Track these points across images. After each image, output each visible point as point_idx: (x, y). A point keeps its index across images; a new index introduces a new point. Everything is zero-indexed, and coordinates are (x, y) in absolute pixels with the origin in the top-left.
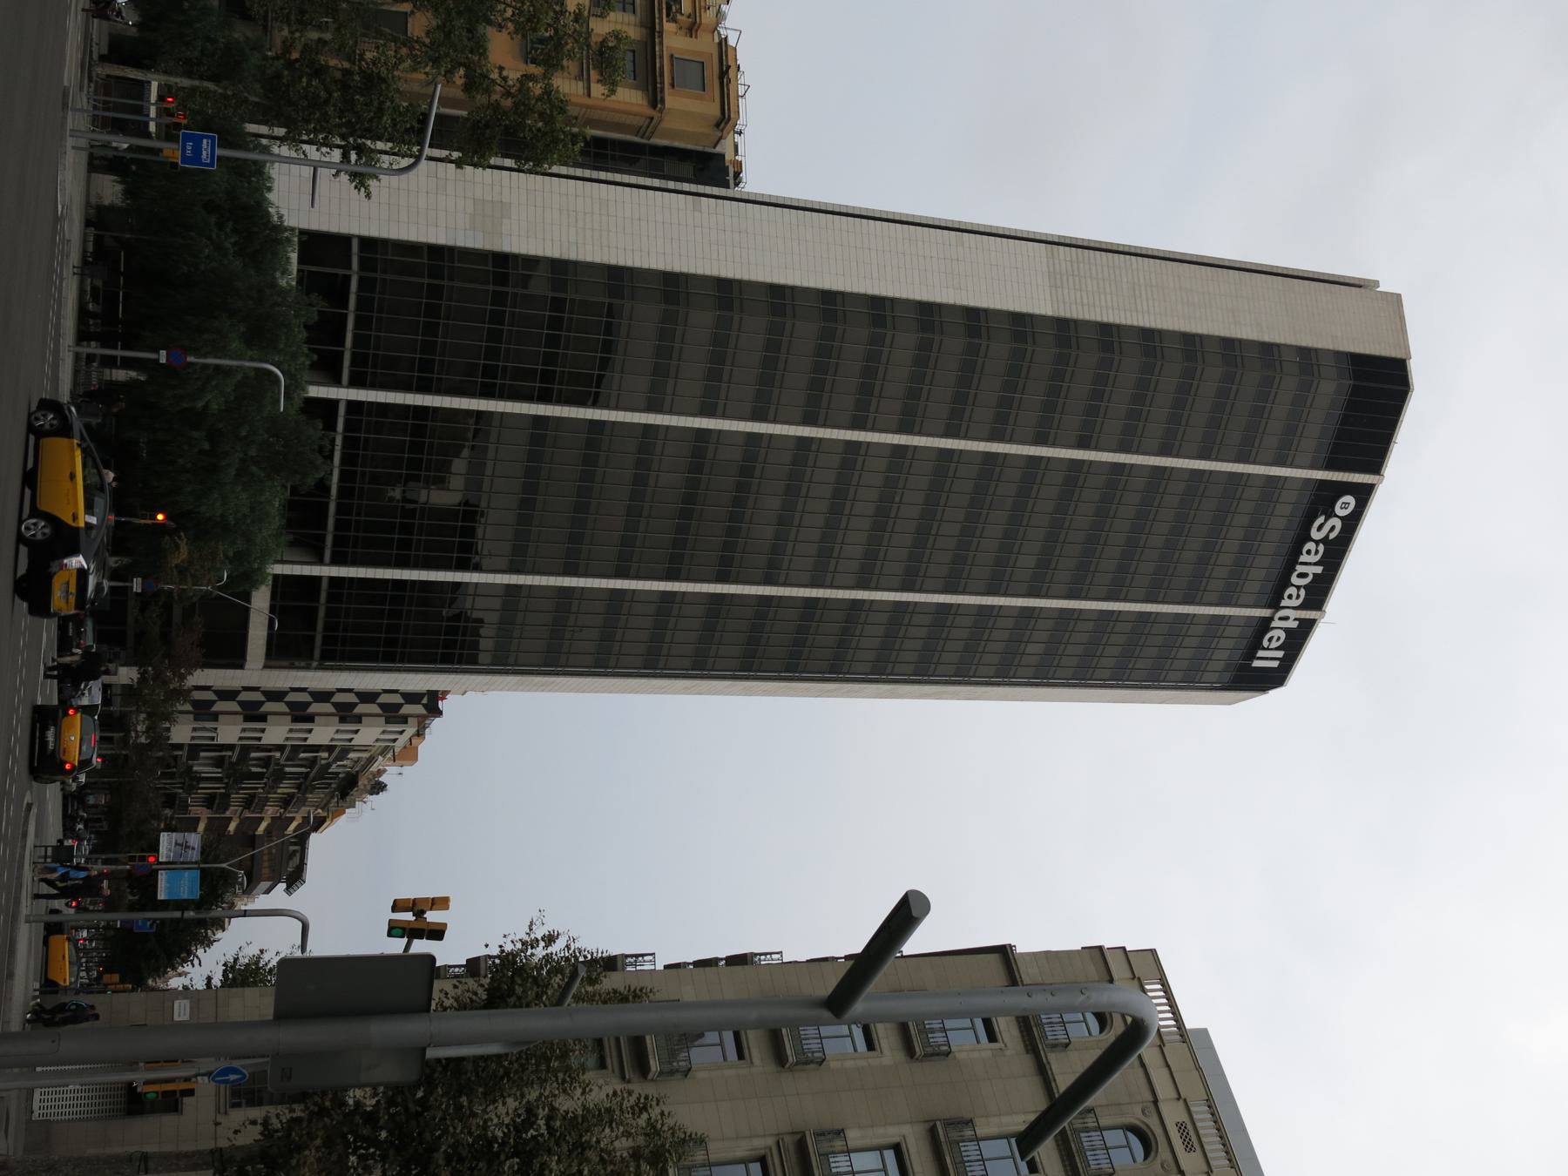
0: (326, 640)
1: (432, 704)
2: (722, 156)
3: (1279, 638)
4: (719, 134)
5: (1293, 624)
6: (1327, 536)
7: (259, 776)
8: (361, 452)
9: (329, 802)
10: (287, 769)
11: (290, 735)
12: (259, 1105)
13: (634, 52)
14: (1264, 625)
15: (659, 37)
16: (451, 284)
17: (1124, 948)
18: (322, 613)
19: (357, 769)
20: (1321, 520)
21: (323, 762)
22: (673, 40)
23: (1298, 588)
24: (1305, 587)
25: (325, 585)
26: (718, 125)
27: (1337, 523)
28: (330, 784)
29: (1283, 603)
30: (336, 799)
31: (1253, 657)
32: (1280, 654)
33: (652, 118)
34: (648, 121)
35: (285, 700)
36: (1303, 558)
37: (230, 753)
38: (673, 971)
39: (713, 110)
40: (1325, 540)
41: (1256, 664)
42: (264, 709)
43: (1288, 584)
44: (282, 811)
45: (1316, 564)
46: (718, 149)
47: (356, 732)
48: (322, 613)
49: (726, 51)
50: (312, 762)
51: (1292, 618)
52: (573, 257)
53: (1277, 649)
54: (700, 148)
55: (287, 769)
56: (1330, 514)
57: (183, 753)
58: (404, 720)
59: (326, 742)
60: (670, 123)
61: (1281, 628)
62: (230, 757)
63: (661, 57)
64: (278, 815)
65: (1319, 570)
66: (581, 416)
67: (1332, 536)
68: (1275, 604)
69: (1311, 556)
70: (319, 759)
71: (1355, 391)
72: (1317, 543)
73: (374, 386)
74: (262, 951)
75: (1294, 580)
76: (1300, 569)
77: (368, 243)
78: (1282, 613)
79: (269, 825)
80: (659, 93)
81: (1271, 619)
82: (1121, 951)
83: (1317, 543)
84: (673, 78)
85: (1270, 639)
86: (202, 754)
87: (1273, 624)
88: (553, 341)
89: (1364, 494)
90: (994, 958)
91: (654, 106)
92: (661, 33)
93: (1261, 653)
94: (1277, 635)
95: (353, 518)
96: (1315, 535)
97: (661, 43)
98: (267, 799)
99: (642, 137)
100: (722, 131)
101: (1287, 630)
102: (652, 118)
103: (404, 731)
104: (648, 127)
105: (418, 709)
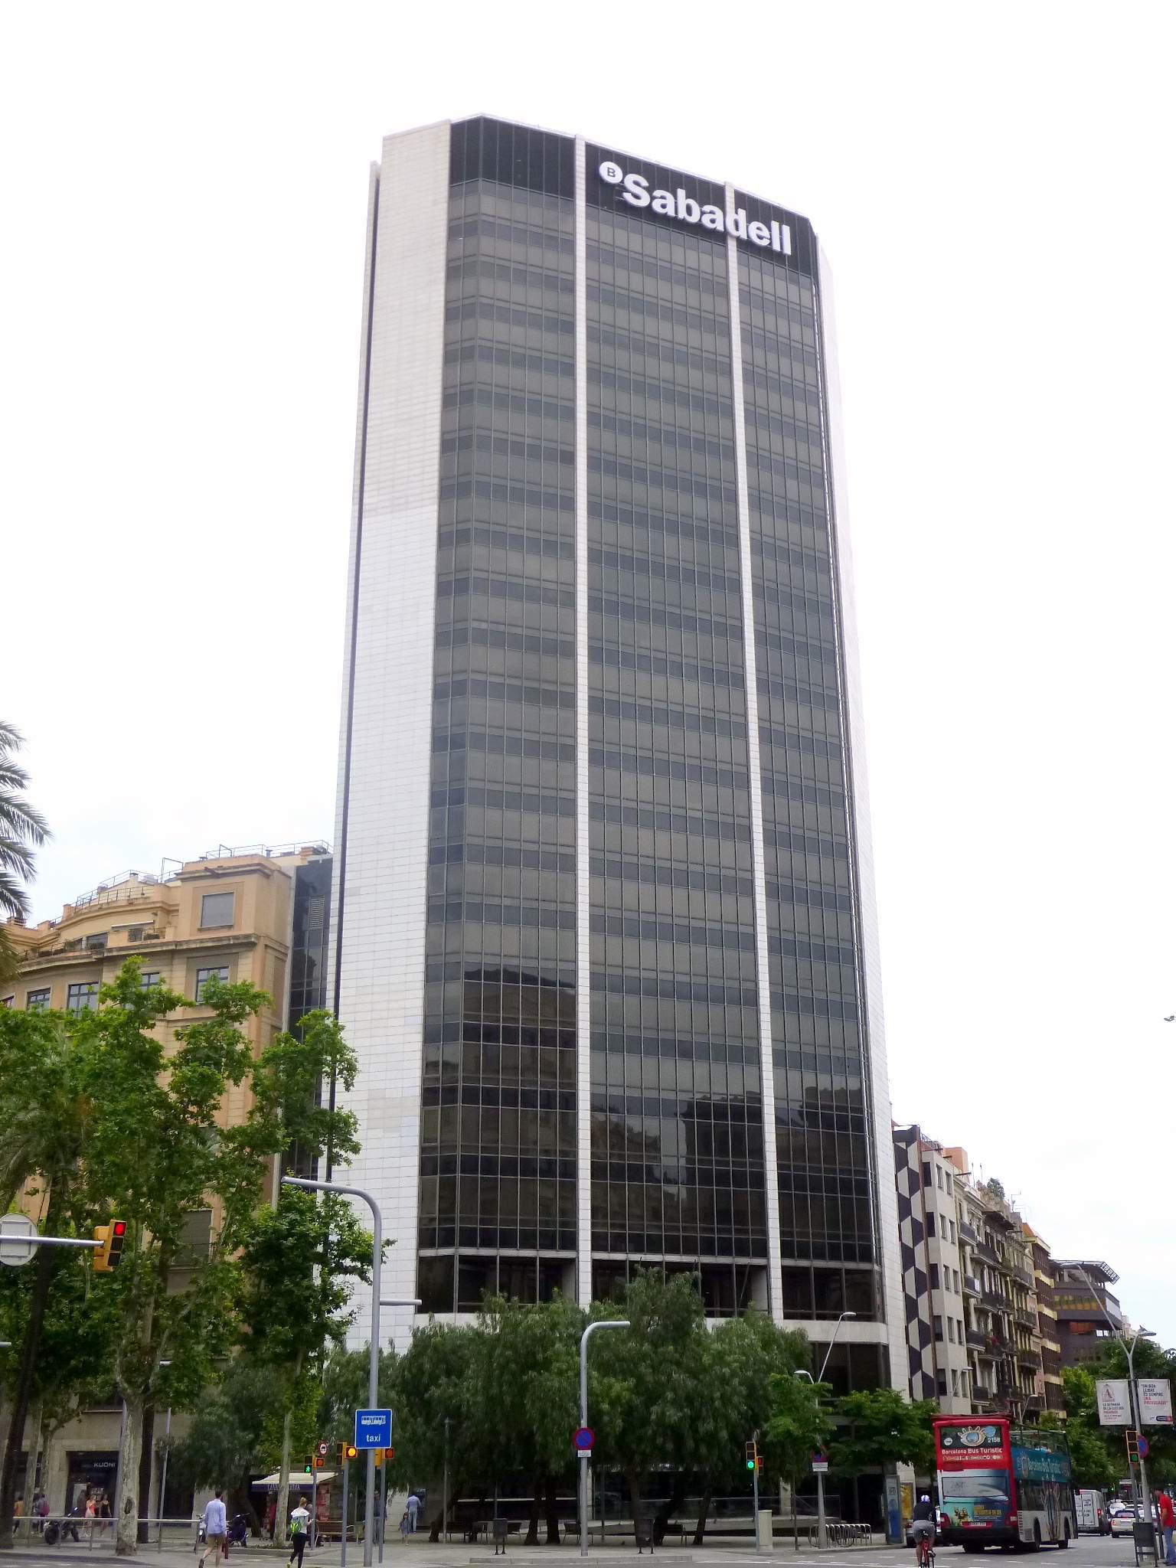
0: (850, 1257)
2: (298, 869)
3: (758, 229)
4: (276, 873)
5: (742, 213)
6: (644, 188)
7: (997, 1321)
9: (1017, 1242)
11: (960, 1393)
15: (181, 945)
16: (458, 1221)
20: (628, 197)
23: (703, 213)
24: (701, 205)
25: (790, 1262)
26: (267, 876)
27: (631, 178)
28: (998, 1242)
29: (721, 228)
30: (1013, 1234)
31: (779, 257)
32: (775, 225)
34: (269, 950)
35: (918, 1349)
36: (671, 212)
37: (976, 1353)
39: (252, 882)
40: (650, 190)
41: (788, 250)
42: (931, 1373)
44: (1030, 1292)
45: (676, 198)
46: (292, 873)
47: (943, 1217)
51: (736, 216)
52: (419, 1021)
53: (770, 229)
55: (987, 1290)
56: (621, 188)
57: (980, 1403)
58: (926, 1167)
63: (202, 941)
64: (1035, 1296)
65: (681, 193)
67: (645, 183)
68: (721, 237)
69: (669, 203)
71: (489, 175)
72: (653, 198)
75: (694, 219)
79: (1044, 1273)
80: (239, 941)
81: (738, 239)
83: (653, 198)
84: (222, 927)
85: (760, 238)
86: (979, 1384)
88: (510, 1035)
89: (597, 156)
91: (254, 944)
92: (177, 943)
93: (776, 247)
94: (755, 231)
96: (644, 202)
97: (187, 942)
98: (1020, 1310)
100: (273, 871)
101: (749, 221)
102: (266, 946)
103: (945, 1266)
105: (913, 1151)
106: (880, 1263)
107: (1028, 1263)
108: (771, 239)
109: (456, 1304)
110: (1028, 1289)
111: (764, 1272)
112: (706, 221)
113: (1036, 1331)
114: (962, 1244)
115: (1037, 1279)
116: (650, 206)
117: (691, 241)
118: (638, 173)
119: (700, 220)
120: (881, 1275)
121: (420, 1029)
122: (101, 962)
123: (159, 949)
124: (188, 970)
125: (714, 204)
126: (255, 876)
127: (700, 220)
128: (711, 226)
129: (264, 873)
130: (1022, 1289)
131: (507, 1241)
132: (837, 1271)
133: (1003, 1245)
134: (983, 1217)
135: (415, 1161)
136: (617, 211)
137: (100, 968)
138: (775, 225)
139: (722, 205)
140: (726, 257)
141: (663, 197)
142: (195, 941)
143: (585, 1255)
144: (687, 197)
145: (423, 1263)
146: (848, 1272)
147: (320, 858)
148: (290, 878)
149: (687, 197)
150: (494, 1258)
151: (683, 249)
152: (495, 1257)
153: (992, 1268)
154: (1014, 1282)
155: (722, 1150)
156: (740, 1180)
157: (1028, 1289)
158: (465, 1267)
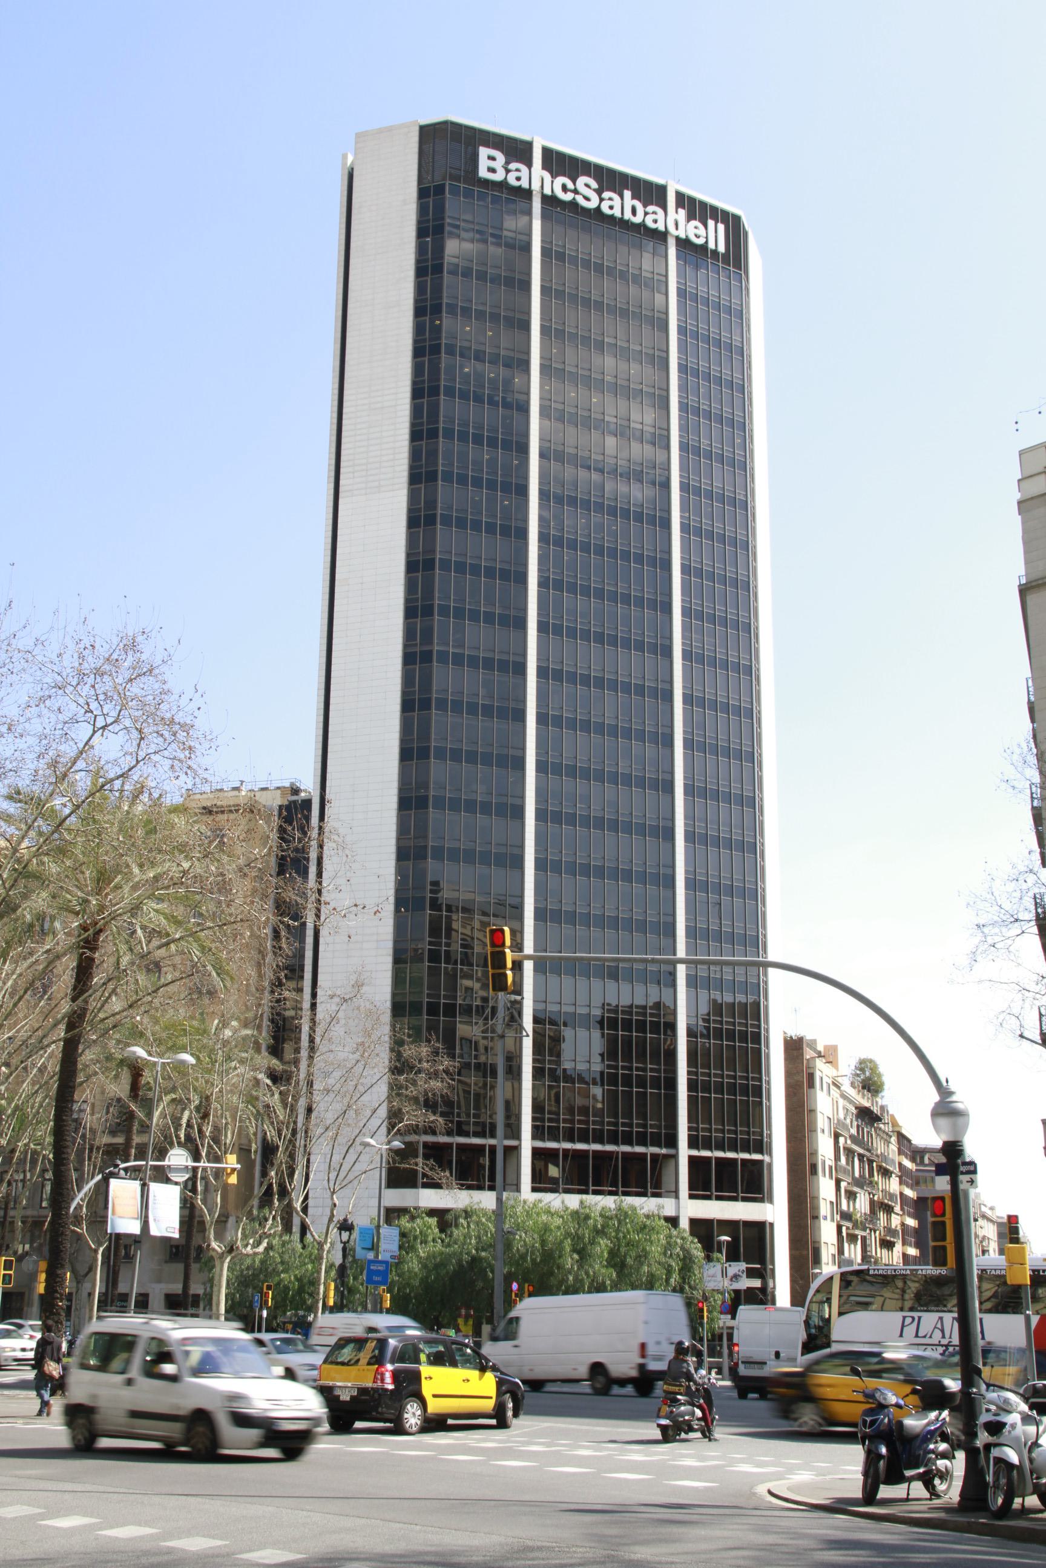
1: (794, 1047)
3: (696, 228)
5: (682, 213)
6: (595, 190)
10: (857, 1174)
12: (647, 1289)
14: (684, 244)
17: (1019, 481)
18: (720, 1154)
21: (849, 1142)
23: (646, 214)
24: (645, 206)
25: (695, 1153)
28: (868, 1132)
29: (662, 228)
31: (715, 252)
32: (711, 223)
36: (617, 213)
37: (844, 1229)
38: (1037, 716)
40: (599, 192)
41: (722, 249)
43: (642, 225)
45: (622, 197)
48: (720, 1154)
50: (849, 1152)
52: (390, 945)
53: (706, 226)
55: (857, 1174)
59: (832, 1141)
61: (552, 182)
62: (848, 1228)
64: (897, 1179)
68: (661, 236)
72: (601, 200)
74: (242, 782)
75: (638, 219)
76: (628, 215)
81: (678, 239)
82: (1022, 483)
83: (601, 200)
85: (697, 236)
87: (683, 236)
90: (1031, 599)
93: (711, 245)
94: (557, 186)
96: (592, 204)
106: (770, 1154)
107: (894, 1147)
108: (707, 238)
110: (892, 1173)
112: (512, 180)
113: (897, 1209)
114: (837, 1136)
115: (900, 1164)
116: (598, 209)
119: (506, 178)
120: (770, 1165)
121: (390, 951)
125: (657, 205)
127: (644, 221)
130: (886, 1173)
133: (872, 1135)
134: (854, 1111)
138: (711, 223)
143: (527, 1144)
144: (633, 198)
149: (633, 198)
150: (484, 1146)
151: (651, 256)
152: (452, 1144)
153: (861, 1157)
154: (880, 1168)
155: (628, 1057)
157: (892, 1173)
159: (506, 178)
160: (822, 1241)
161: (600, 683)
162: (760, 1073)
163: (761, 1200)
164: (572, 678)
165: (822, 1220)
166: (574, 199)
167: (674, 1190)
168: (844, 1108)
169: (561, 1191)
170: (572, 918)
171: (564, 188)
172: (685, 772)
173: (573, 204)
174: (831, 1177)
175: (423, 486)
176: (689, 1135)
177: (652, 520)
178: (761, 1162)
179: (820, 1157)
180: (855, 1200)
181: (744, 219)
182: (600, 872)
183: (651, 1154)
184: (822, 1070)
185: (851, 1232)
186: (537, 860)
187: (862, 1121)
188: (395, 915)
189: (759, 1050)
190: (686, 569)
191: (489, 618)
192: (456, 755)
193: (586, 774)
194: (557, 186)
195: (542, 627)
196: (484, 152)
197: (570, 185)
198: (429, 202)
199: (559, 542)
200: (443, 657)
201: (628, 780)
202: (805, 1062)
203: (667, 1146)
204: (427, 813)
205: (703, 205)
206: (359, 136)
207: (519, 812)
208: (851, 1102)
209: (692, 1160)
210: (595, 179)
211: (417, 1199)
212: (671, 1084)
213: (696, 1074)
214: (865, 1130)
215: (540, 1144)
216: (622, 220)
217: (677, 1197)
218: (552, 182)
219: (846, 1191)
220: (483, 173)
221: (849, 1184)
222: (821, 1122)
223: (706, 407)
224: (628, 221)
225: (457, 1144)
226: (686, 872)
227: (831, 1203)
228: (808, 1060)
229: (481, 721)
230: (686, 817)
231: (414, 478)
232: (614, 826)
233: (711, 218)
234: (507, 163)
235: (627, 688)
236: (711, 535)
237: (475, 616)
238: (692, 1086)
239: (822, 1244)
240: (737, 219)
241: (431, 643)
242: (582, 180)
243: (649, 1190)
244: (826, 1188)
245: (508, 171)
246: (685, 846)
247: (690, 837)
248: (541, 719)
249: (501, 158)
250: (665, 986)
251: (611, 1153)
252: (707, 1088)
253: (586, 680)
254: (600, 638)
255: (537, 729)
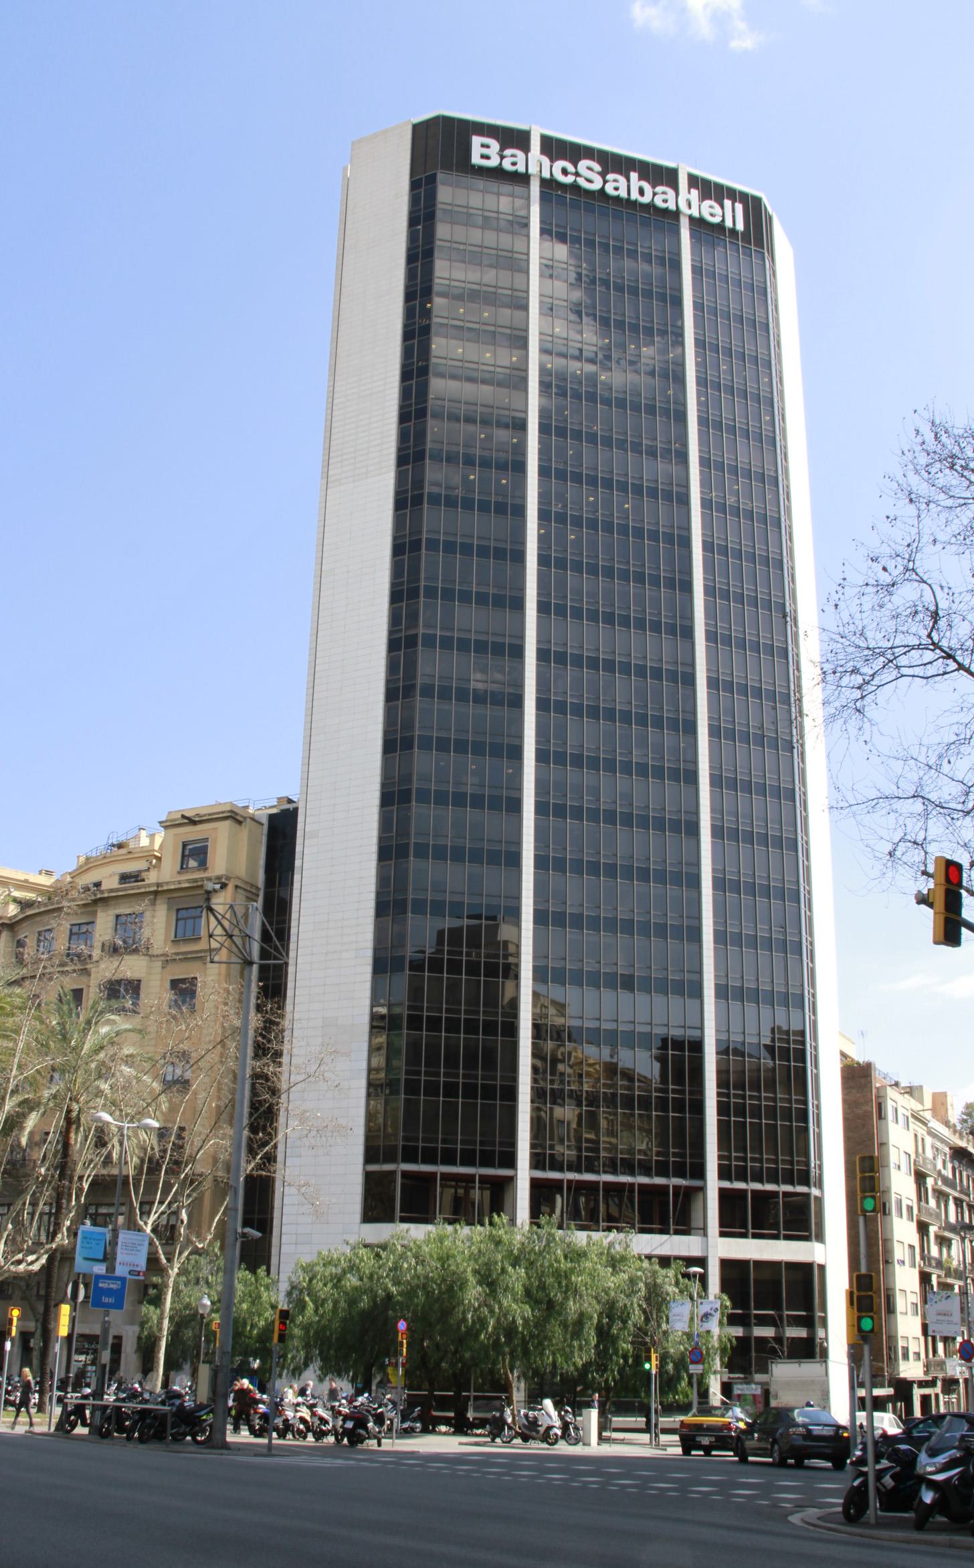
2: (271, 817)
3: (711, 207)
4: (248, 820)
5: (695, 193)
6: (599, 173)
8: (421, 1144)
13: (178, 910)
14: (698, 223)
18: (757, 1186)
19: (947, 1149)
21: (940, 1183)
22: (167, 873)
23: (655, 194)
24: (654, 187)
25: (539, 1174)
26: (240, 823)
29: (672, 207)
31: (733, 232)
32: (728, 203)
33: (237, 887)
34: (239, 890)
36: (623, 193)
39: (225, 826)
40: (603, 174)
41: (740, 227)
43: (651, 207)
45: (628, 180)
46: (265, 821)
49: (171, 821)
50: (941, 1195)
51: (688, 196)
52: (369, 953)
54: (264, 839)
60: (242, 870)
61: (551, 167)
62: (939, 1276)
63: (179, 882)
66: (711, 953)
67: (597, 168)
68: (522, 179)
69: (617, 185)
70: (936, 1187)
72: (605, 182)
73: (512, 1143)
75: (646, 199)
76: (635, 195)
77: (371, 1155)
78: (683, 207)
81: (691, 218)
83: (605, 182)
85: (712, 215)
87: (696, 214)
92: (158, 885)
93: (729, 223)
94: (558, 169)
95: (478, 1148)
96: (597, 185)
97: (167, 883)
99: (258, 896)
100: (245, 818)
102: (237, 887)
104: (244, 889)
106: (820, 1185)
108: (723, 216)
109: (398, 1214)
111: (701, 1195)
112: (658, 202)
116: (602, 190)
117: (493, 186)
118: (592, 159)
119: (501, 164)
120: (819, 1201)
122: (96, 902)
123: (143, 890)
124: (169, 909)
125: (668, 185)
126: (227, 823)
128: (664, 206)
129: (236, 819)
131: (449, 1159)
132: (775, 1194)
134: (947, 1150)
135: (363, 1083)
136: (457, 171)
137: (95, 908)
138: (728, 203)
139: (674, 186)
140: (528, 198)
141: (615, 181)
142: (173, 883)
143: (524, 1173)
144: (640, 179)
145: (369, 1177)
146: (786, 1194)
147: (291, 806)
148: (262, 824)
149: (640, 179)
150: (435, 1174)
156: (679, 1106)
158: (406, 1181)
159: (501, 164)
160: (898, 1288)
161: (610, 666)
162: (805, 1094)
163: (807, 1238)
164: (578, 661)
165: (897, 1266)
166: (575, 181)
167: (702, 1226)
168: (933, 1147)
169: (672, 1232)
170: (577, 921)
171: (565, 172)
172: (711, 761)
173: (575, 187)
174: (911, 1218)
175: (410, 466)
176: (719, 1165)
177: (668, 496)
178: (807, 1195)
179: (894, 1197)
180: (949, 1247)
181: (765, 201)
182: (611, 871)
183: (674, 1186)
184: (895, 1101)
185: (943, 1280)
186: (537, 857)
187: (960, 1162)
188: (376, 921)
189: (804, 1069)
190: (708, 547)
191: (482, 599)
192: (443, 745)
193: (594, 764)
194: (558, 169)
195: (543, 608)
196: (476, 141)
197: (571, 168)
198: (420, 193)
199: (561, 518)
200: (429, 641)
201: (643, 770)
202: (874, 1091)
203: (693, 1177)
204: (409, 809)
205: (719, 187)
206: (353, 143)
207: (516, 806)
208: (943, 1141)
209: (723, 1193)
210: (599, 162)
211: (812, 1253)
212: (698, 1107)
213: (728, 1095)
214: (964, 1174)
215: (539, 1174)
216: (628, 200)
217: (705, 1235)
218: (551, 167)
219: (937, 1237)
220: (476, 159)
221: (940, 1228)
222: (894, 1157)
223: (772, 473)
224: (636, 201)
225: (441, 1174)
226: (714, 870)
227: (912, 1247)
228: (878, 1089)
229: (472, 709)
230: (713, 810)
231: (402, 460)
232: (628, 820)
233: (728, 198)
234: (502, 149)
235: (641, 671)
236: (736, 511)
237: (465, 597)
238: (722, 1109)
239: (898, 1292)
240: (757, 201)
241: (416, 626)
242: (583, 164)
243: (672, 1227)
244: (903, 1232)
245: (502, 157)
246: (712, 842)
247: (717, 832)
248: (542, 705)
249: (495, 145)
250: (690, 996)
251: (623, 1184)
252: (741, 1110)
253: (594, 663)
254: (609, 619)
255: (537, 716)
